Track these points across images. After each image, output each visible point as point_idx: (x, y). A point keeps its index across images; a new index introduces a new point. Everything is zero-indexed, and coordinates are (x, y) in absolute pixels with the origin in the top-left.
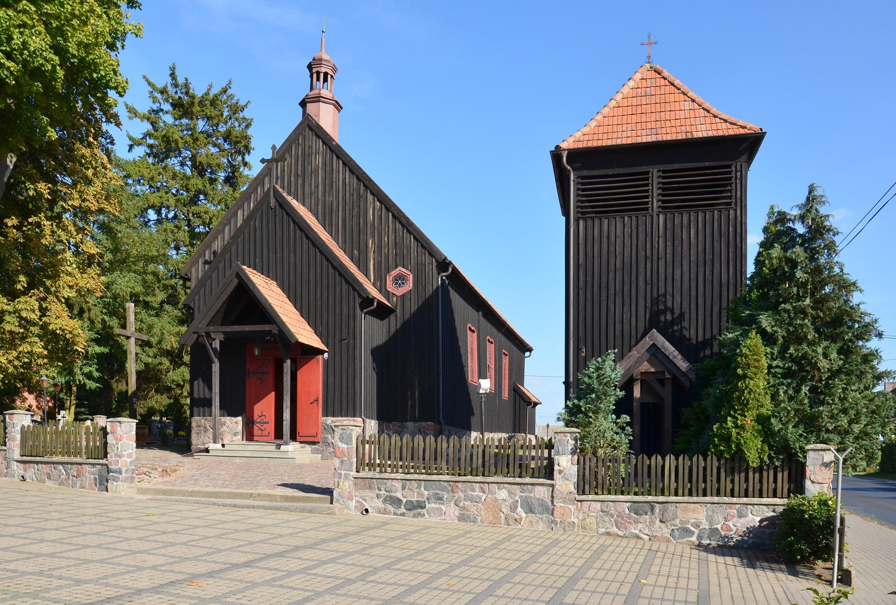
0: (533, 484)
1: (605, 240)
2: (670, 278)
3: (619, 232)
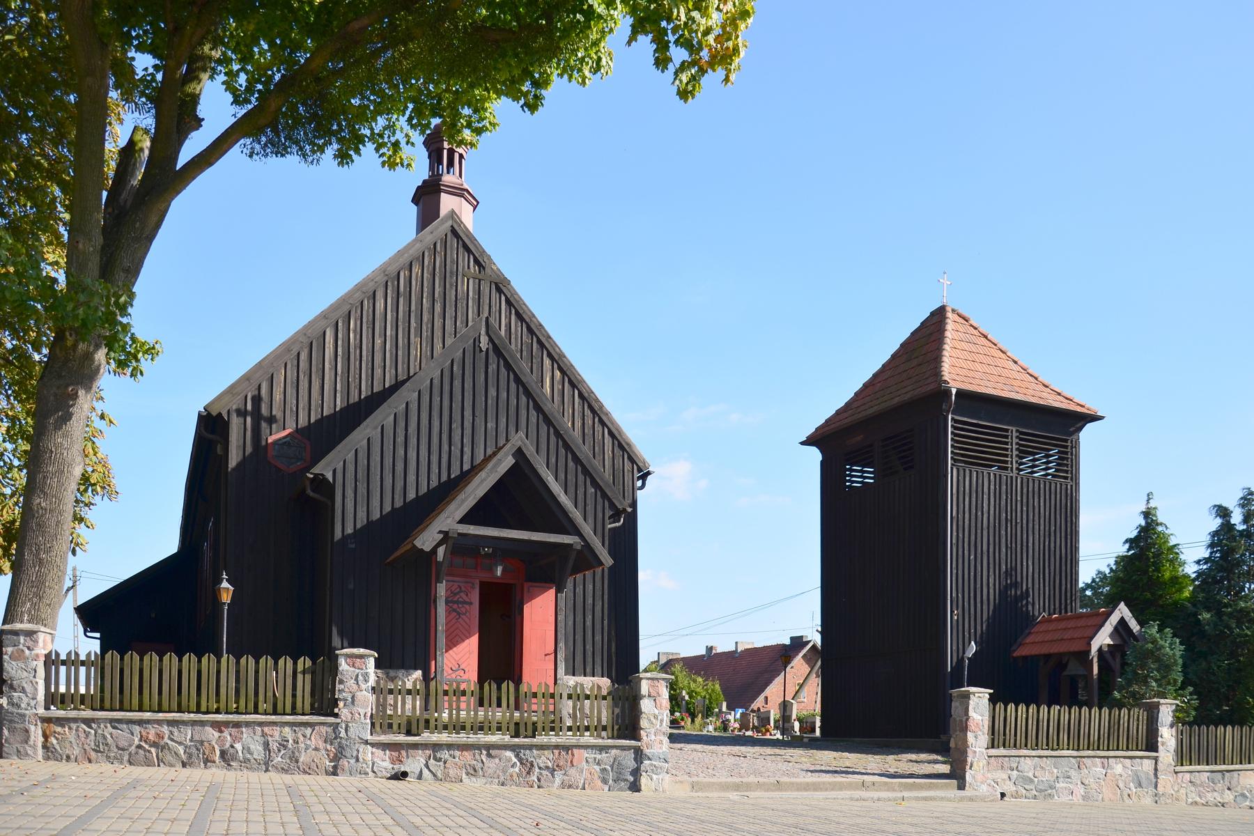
0: (1141, 758)
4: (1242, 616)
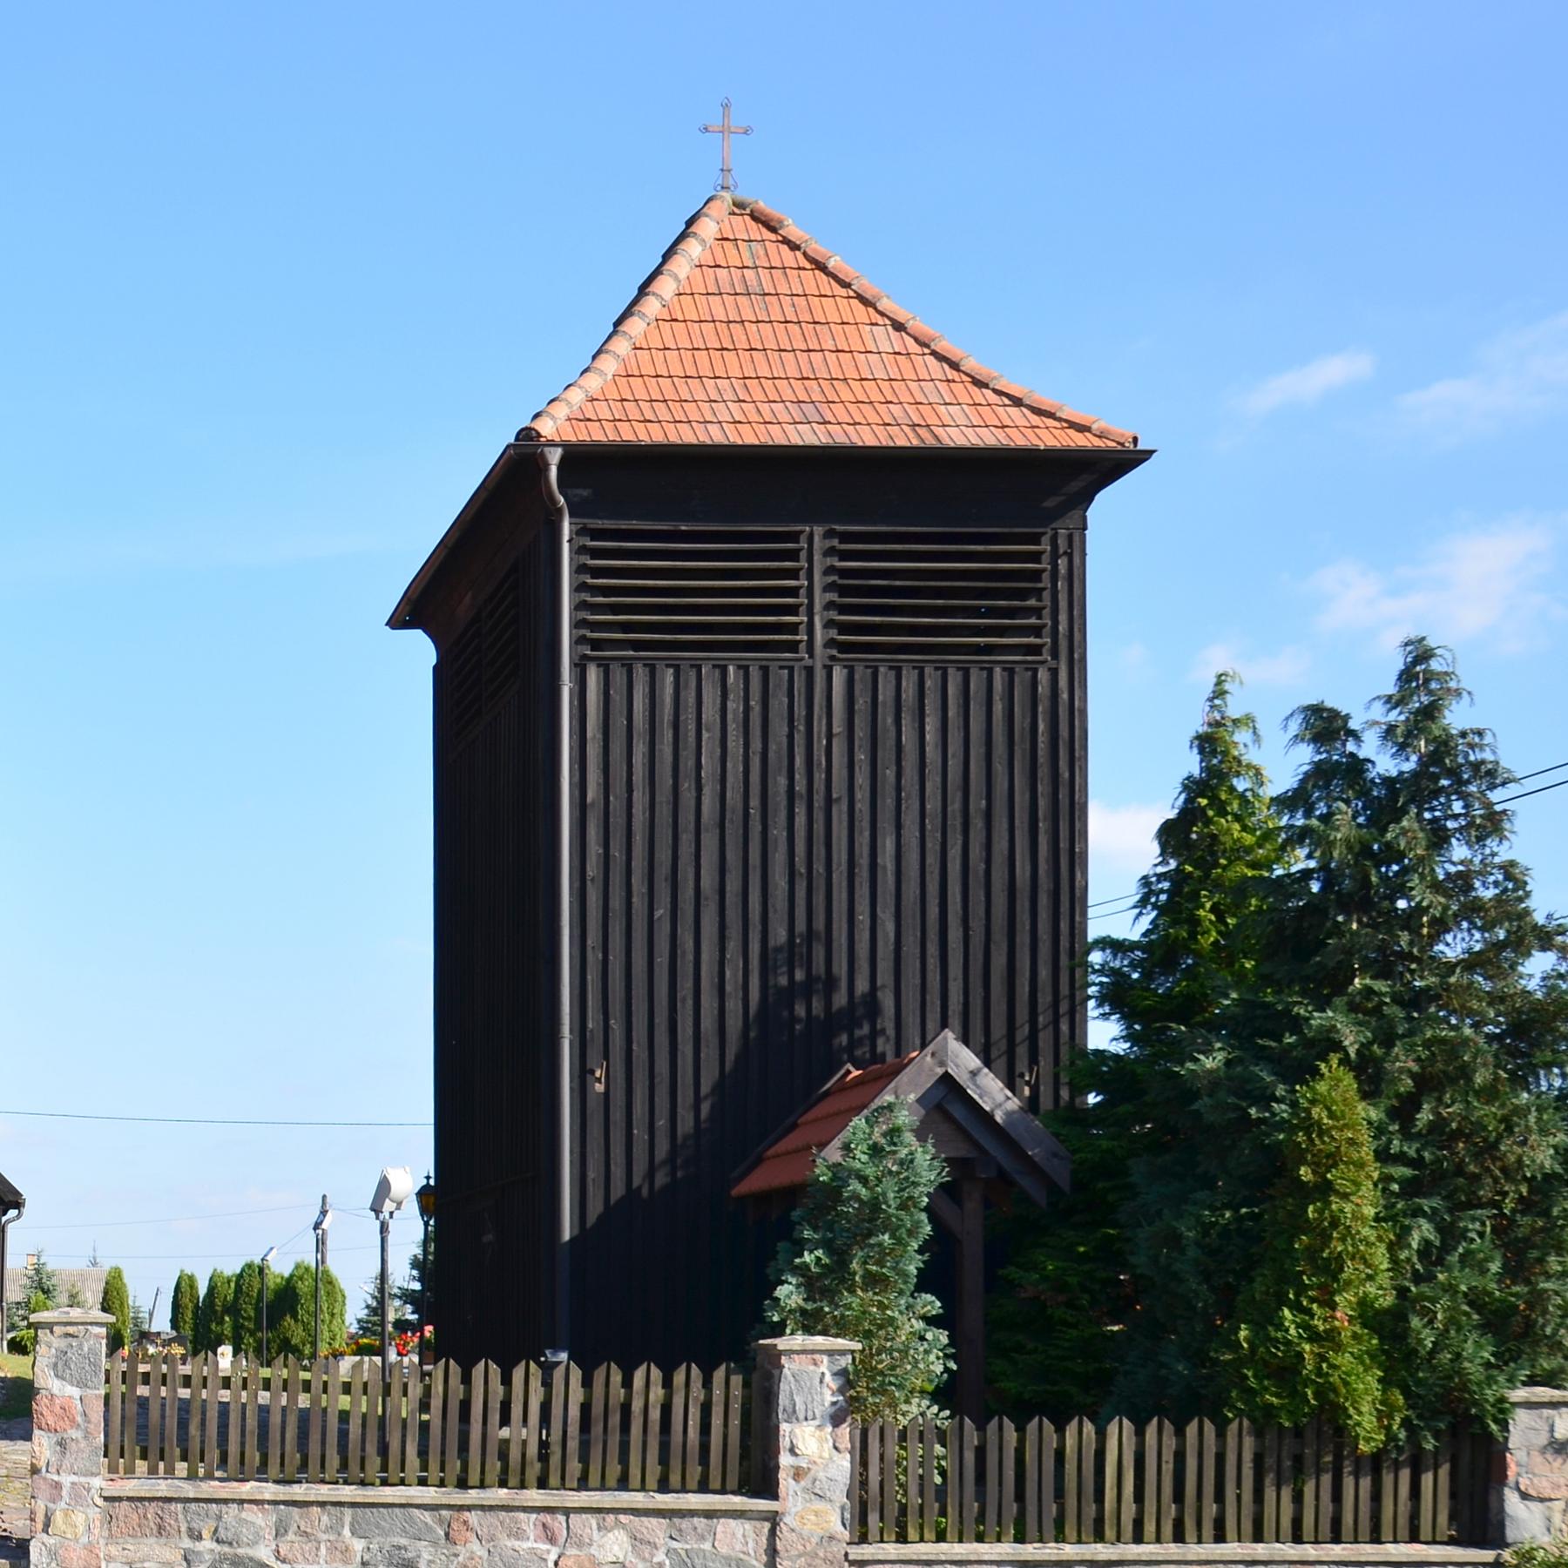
0: (710, 1514)
1: (668, 735)
2: (863, 861)
3: (710, 712)
4: (1531, 1031)
